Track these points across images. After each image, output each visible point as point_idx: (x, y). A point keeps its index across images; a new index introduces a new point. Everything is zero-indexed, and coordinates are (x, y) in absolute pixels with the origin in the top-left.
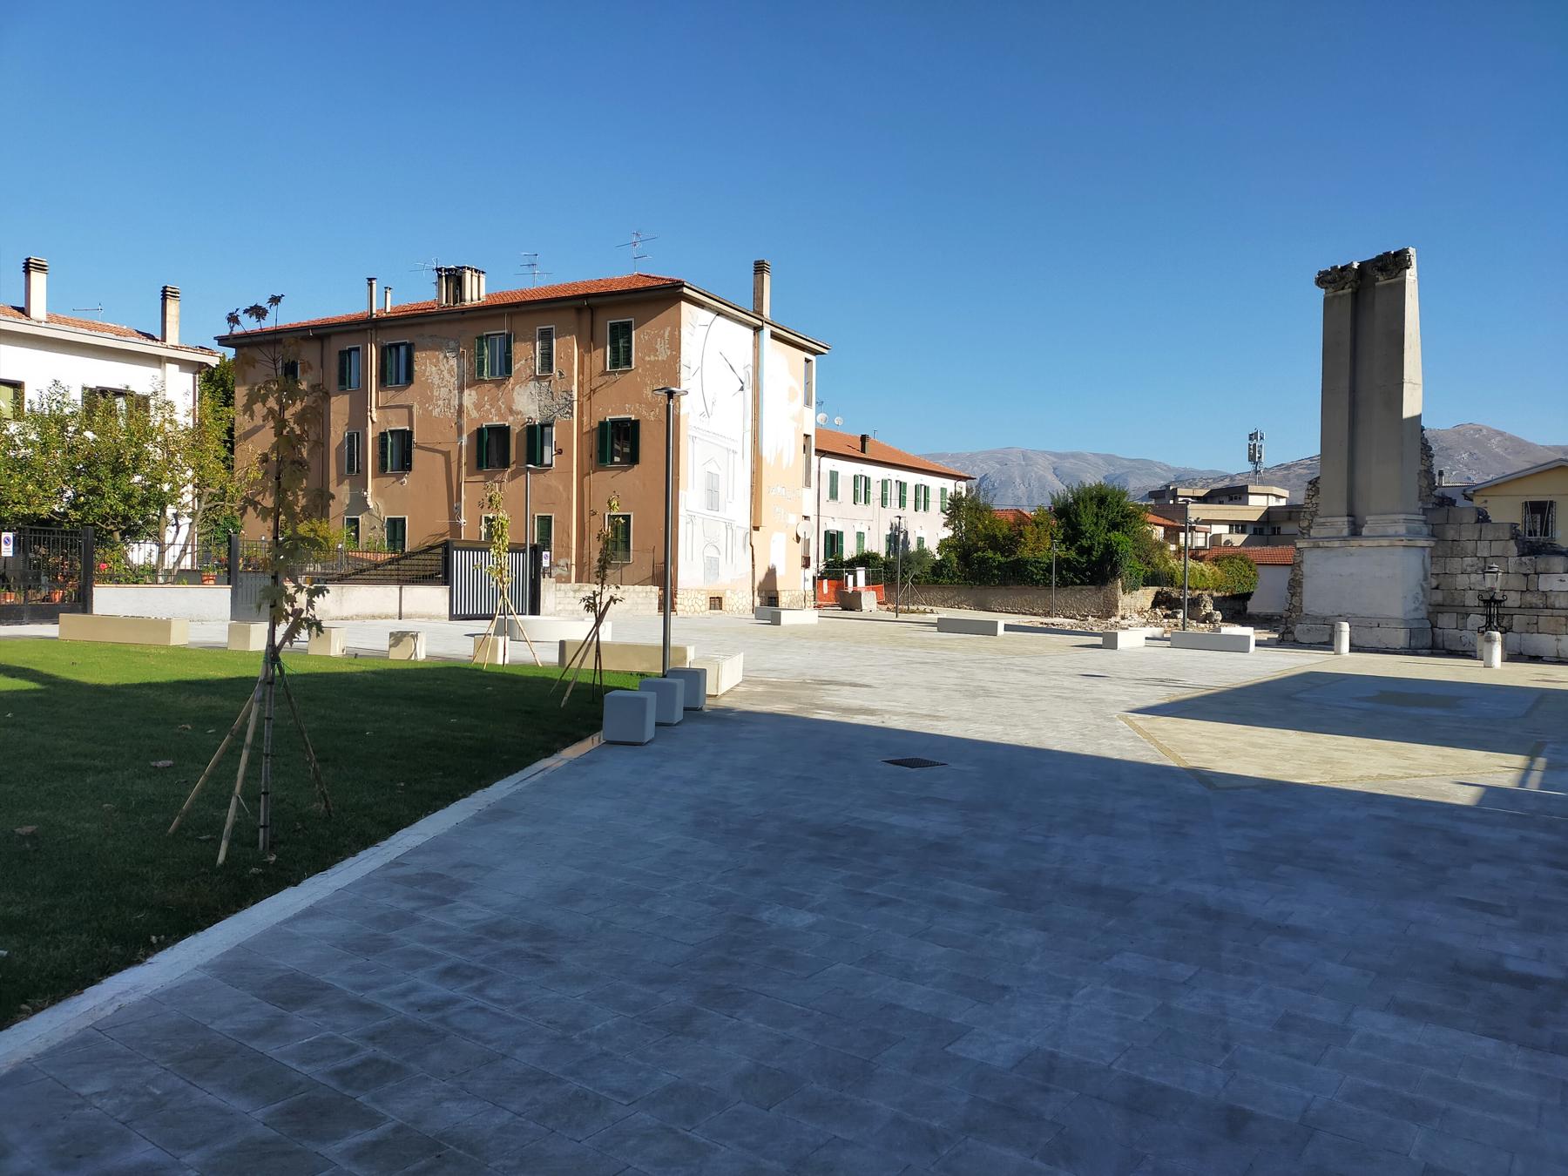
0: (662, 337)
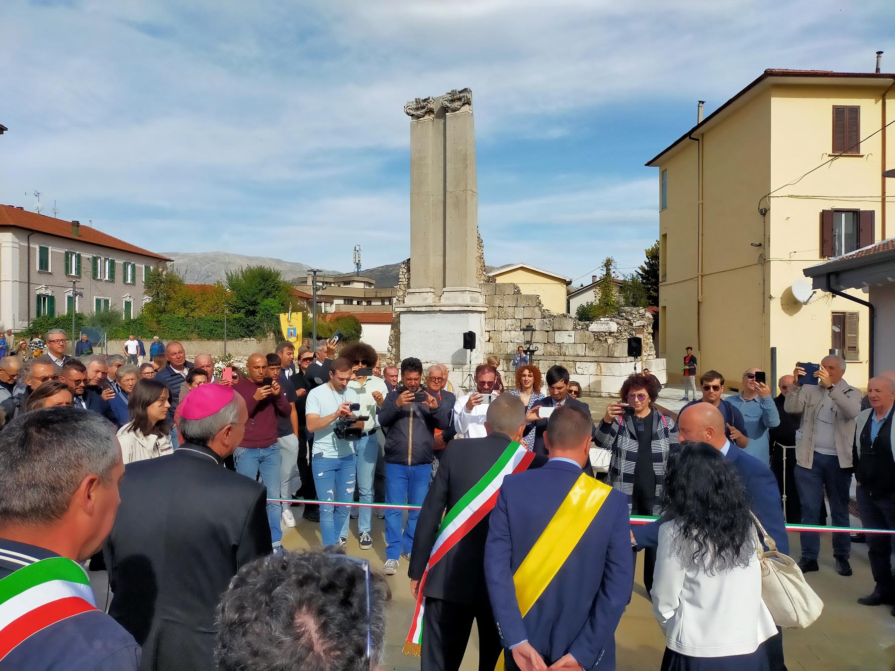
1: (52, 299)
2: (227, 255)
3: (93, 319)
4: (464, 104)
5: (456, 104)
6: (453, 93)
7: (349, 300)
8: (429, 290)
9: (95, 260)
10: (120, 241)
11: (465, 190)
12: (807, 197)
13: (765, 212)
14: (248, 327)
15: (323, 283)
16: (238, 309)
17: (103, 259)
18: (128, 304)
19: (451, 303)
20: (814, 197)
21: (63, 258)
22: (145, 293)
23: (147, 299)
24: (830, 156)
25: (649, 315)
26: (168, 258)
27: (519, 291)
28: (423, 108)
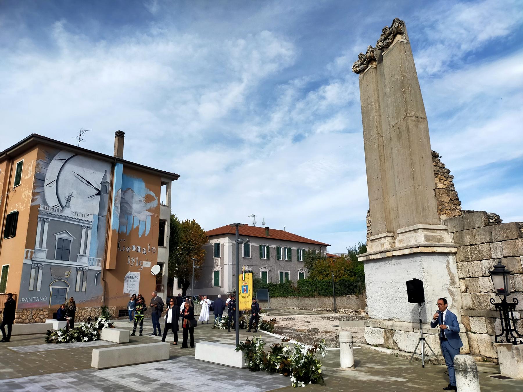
9: (278, 249)
14: (349, 287)
17: (283, 248)
18: (264, 273)
21: (259, 249)
25: (435, 70)
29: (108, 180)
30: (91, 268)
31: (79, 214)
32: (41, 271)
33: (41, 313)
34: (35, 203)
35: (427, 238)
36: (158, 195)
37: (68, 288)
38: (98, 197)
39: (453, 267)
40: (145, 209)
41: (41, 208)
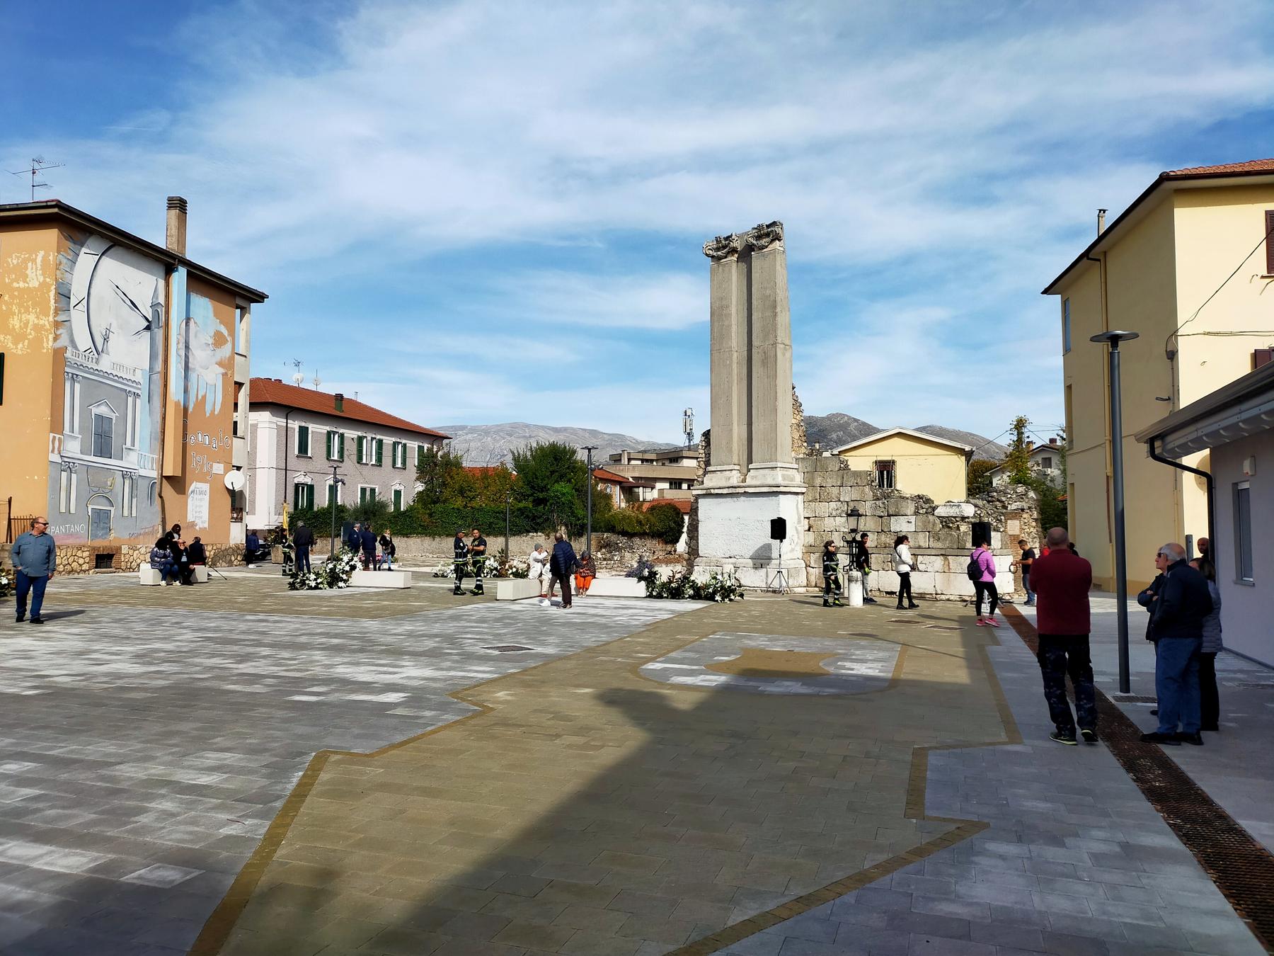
0: (34, 261)
1: (311, 488)
2: (527, 426)
3: (356, 510)
4: (773, 241)
5: (764, 241)
6: (760, 228)
7: (676, 483)
8: (731, 467)
9: (360, 439)
10: (390, 416)
11: (774, 344)
12: (1231, 334)
13: (1172, 355)
15: (643, 461)
16: (524, 497)
18: (398, 493)
19: (758, 483)
20: (1242, 333)
21: (325, 439)
22: (417, 479)
23: (420, 487)
24: (1263, 277)
26: (442, 432)
27: (847, 466)
28: (724, 247)
29: (162, 300)
30: (142, 472)
31: (121, 366)
32: (74, 476)
33: (79, 554)
34: (59, 344)
35: (784, 477)
36: (232, 332)
37: (113, 510)
38: (147, 334)
39: (801, 506)
40: (214, 360)
41: (68, 355)
